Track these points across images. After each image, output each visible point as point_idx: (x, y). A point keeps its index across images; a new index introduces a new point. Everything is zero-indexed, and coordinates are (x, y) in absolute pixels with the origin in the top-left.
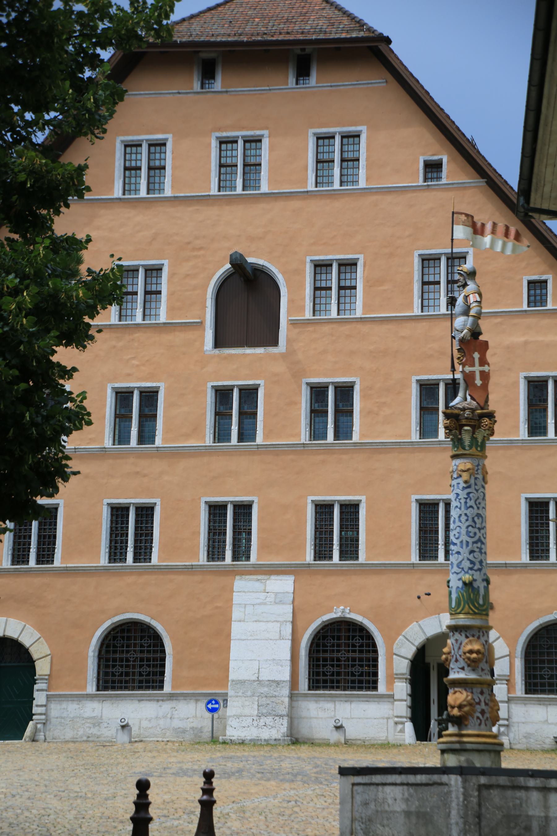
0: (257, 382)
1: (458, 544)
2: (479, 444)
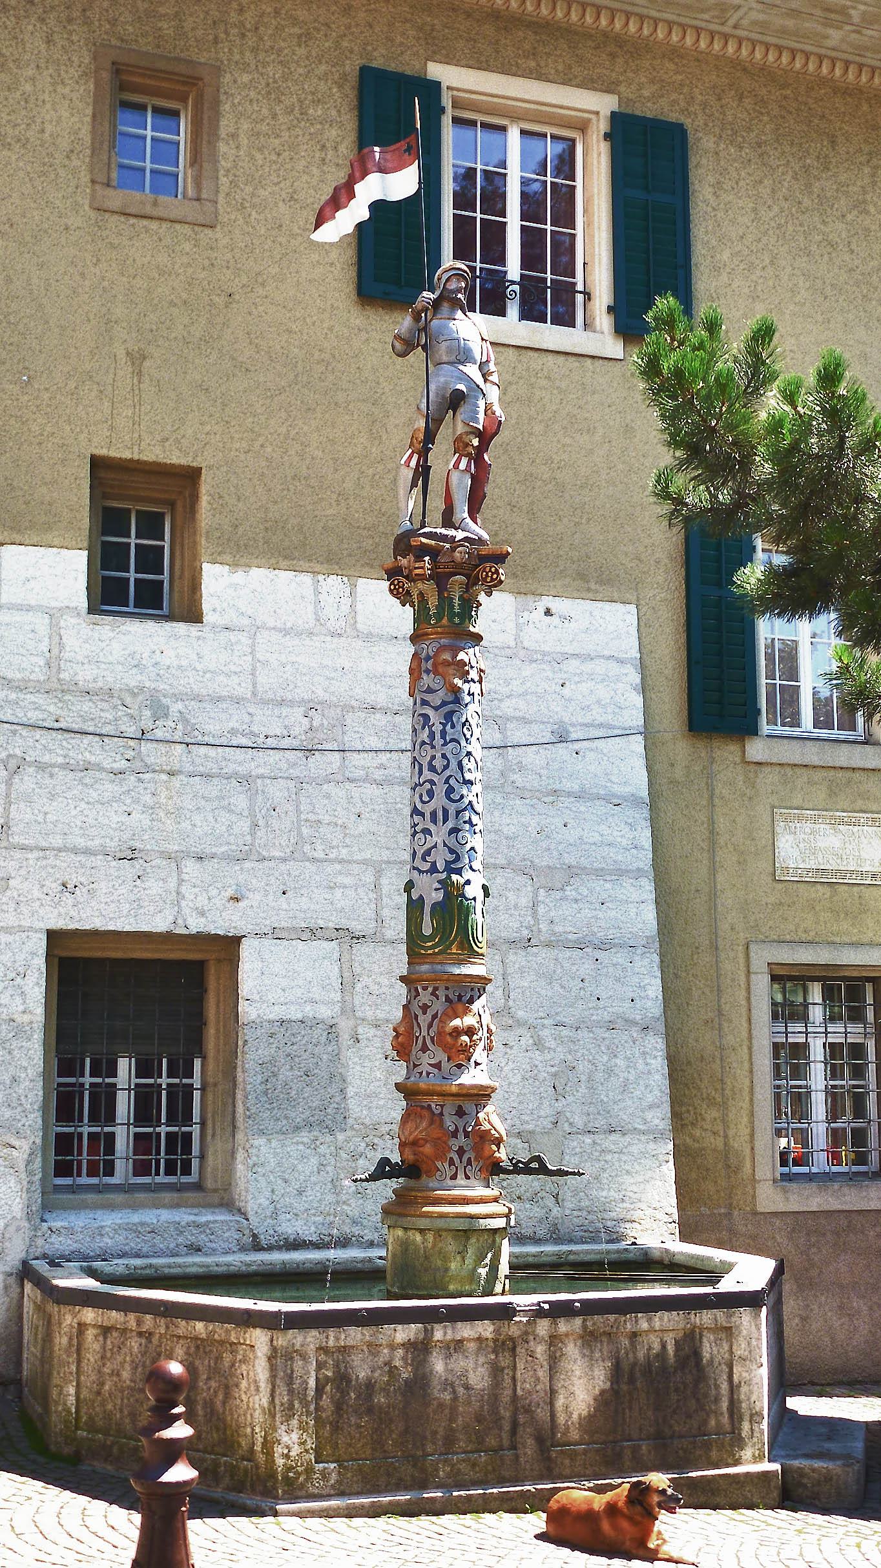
1: (427, 816)
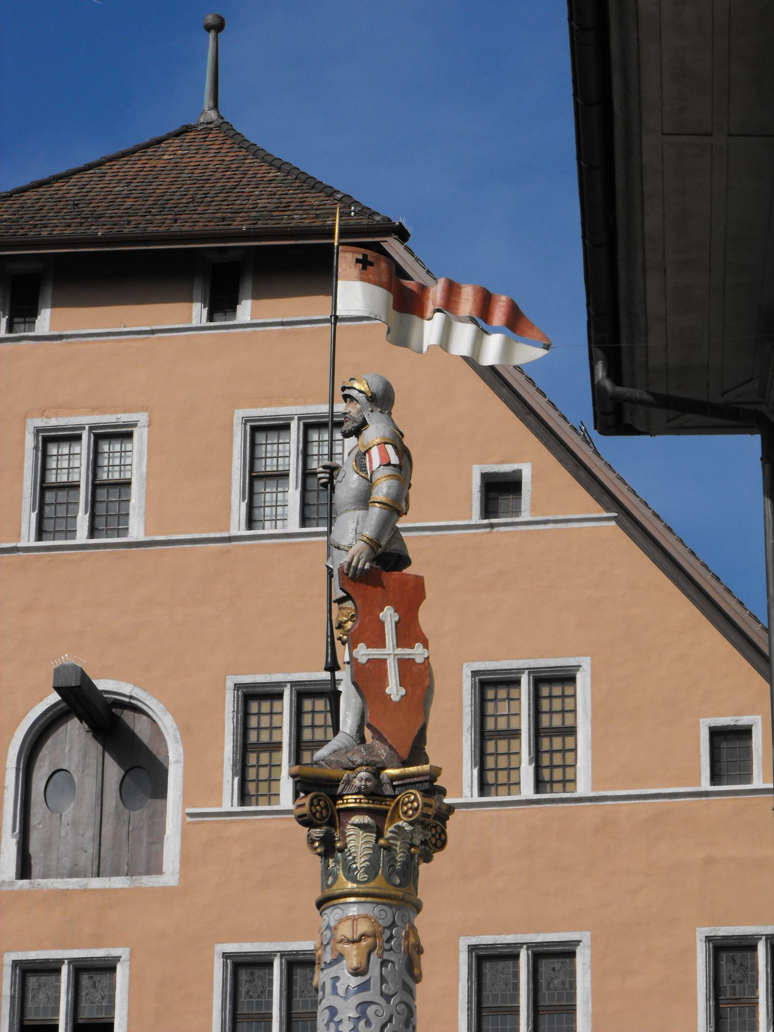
0: (114, 952)
2: (398, 866)
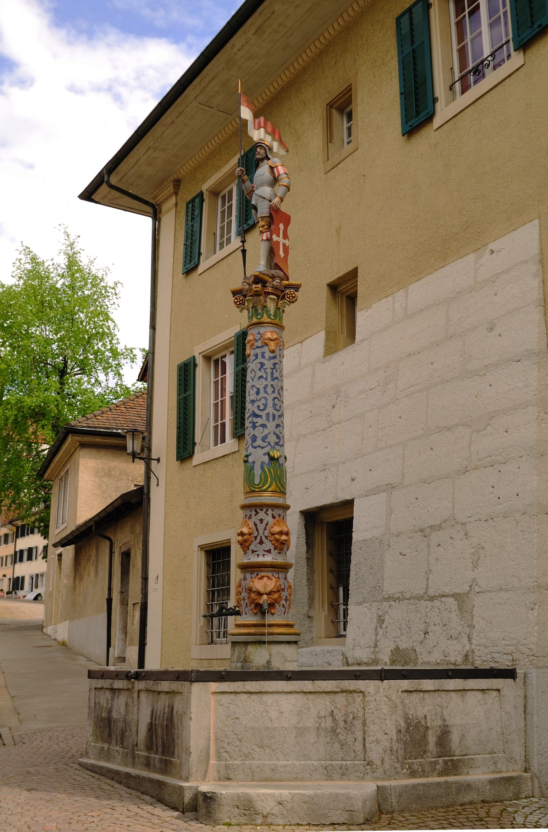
1: (264, 417)
